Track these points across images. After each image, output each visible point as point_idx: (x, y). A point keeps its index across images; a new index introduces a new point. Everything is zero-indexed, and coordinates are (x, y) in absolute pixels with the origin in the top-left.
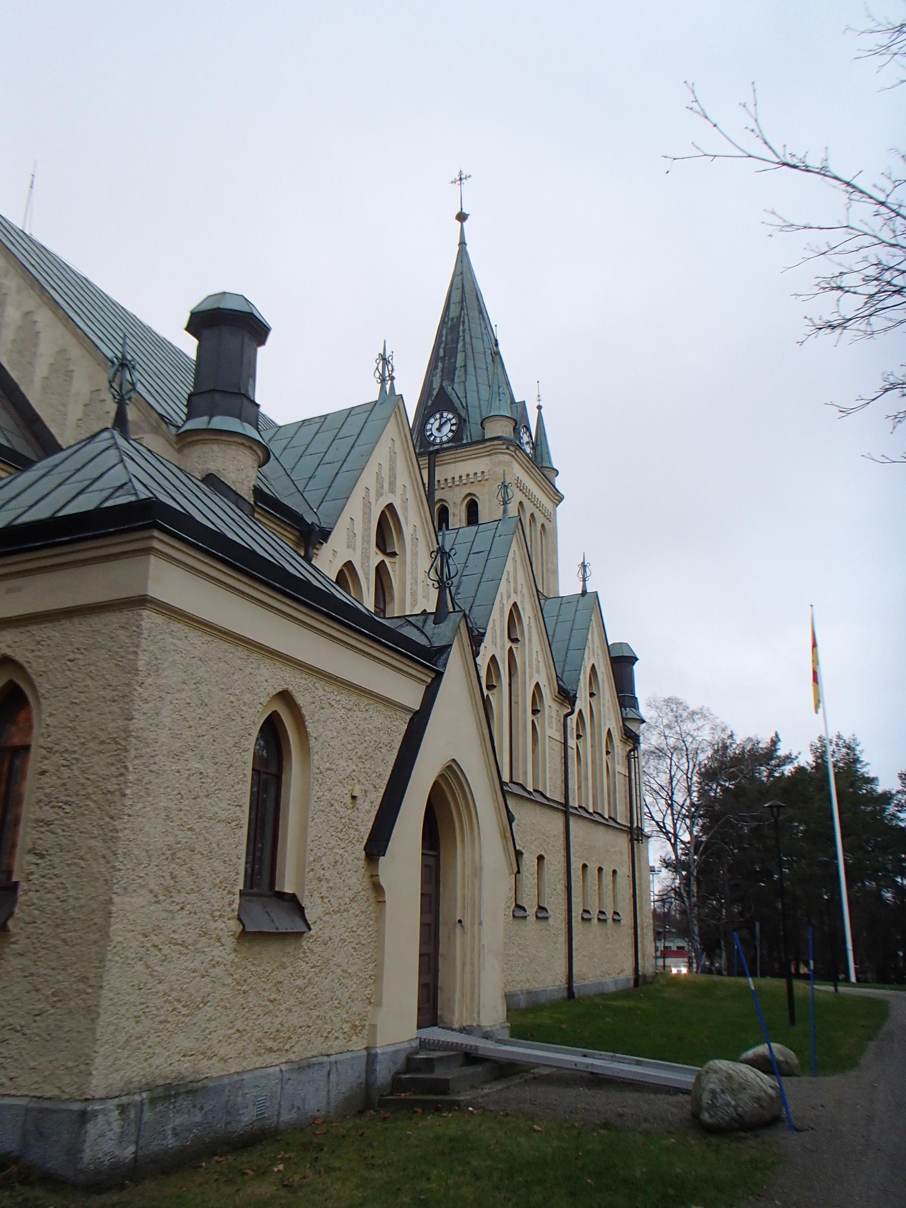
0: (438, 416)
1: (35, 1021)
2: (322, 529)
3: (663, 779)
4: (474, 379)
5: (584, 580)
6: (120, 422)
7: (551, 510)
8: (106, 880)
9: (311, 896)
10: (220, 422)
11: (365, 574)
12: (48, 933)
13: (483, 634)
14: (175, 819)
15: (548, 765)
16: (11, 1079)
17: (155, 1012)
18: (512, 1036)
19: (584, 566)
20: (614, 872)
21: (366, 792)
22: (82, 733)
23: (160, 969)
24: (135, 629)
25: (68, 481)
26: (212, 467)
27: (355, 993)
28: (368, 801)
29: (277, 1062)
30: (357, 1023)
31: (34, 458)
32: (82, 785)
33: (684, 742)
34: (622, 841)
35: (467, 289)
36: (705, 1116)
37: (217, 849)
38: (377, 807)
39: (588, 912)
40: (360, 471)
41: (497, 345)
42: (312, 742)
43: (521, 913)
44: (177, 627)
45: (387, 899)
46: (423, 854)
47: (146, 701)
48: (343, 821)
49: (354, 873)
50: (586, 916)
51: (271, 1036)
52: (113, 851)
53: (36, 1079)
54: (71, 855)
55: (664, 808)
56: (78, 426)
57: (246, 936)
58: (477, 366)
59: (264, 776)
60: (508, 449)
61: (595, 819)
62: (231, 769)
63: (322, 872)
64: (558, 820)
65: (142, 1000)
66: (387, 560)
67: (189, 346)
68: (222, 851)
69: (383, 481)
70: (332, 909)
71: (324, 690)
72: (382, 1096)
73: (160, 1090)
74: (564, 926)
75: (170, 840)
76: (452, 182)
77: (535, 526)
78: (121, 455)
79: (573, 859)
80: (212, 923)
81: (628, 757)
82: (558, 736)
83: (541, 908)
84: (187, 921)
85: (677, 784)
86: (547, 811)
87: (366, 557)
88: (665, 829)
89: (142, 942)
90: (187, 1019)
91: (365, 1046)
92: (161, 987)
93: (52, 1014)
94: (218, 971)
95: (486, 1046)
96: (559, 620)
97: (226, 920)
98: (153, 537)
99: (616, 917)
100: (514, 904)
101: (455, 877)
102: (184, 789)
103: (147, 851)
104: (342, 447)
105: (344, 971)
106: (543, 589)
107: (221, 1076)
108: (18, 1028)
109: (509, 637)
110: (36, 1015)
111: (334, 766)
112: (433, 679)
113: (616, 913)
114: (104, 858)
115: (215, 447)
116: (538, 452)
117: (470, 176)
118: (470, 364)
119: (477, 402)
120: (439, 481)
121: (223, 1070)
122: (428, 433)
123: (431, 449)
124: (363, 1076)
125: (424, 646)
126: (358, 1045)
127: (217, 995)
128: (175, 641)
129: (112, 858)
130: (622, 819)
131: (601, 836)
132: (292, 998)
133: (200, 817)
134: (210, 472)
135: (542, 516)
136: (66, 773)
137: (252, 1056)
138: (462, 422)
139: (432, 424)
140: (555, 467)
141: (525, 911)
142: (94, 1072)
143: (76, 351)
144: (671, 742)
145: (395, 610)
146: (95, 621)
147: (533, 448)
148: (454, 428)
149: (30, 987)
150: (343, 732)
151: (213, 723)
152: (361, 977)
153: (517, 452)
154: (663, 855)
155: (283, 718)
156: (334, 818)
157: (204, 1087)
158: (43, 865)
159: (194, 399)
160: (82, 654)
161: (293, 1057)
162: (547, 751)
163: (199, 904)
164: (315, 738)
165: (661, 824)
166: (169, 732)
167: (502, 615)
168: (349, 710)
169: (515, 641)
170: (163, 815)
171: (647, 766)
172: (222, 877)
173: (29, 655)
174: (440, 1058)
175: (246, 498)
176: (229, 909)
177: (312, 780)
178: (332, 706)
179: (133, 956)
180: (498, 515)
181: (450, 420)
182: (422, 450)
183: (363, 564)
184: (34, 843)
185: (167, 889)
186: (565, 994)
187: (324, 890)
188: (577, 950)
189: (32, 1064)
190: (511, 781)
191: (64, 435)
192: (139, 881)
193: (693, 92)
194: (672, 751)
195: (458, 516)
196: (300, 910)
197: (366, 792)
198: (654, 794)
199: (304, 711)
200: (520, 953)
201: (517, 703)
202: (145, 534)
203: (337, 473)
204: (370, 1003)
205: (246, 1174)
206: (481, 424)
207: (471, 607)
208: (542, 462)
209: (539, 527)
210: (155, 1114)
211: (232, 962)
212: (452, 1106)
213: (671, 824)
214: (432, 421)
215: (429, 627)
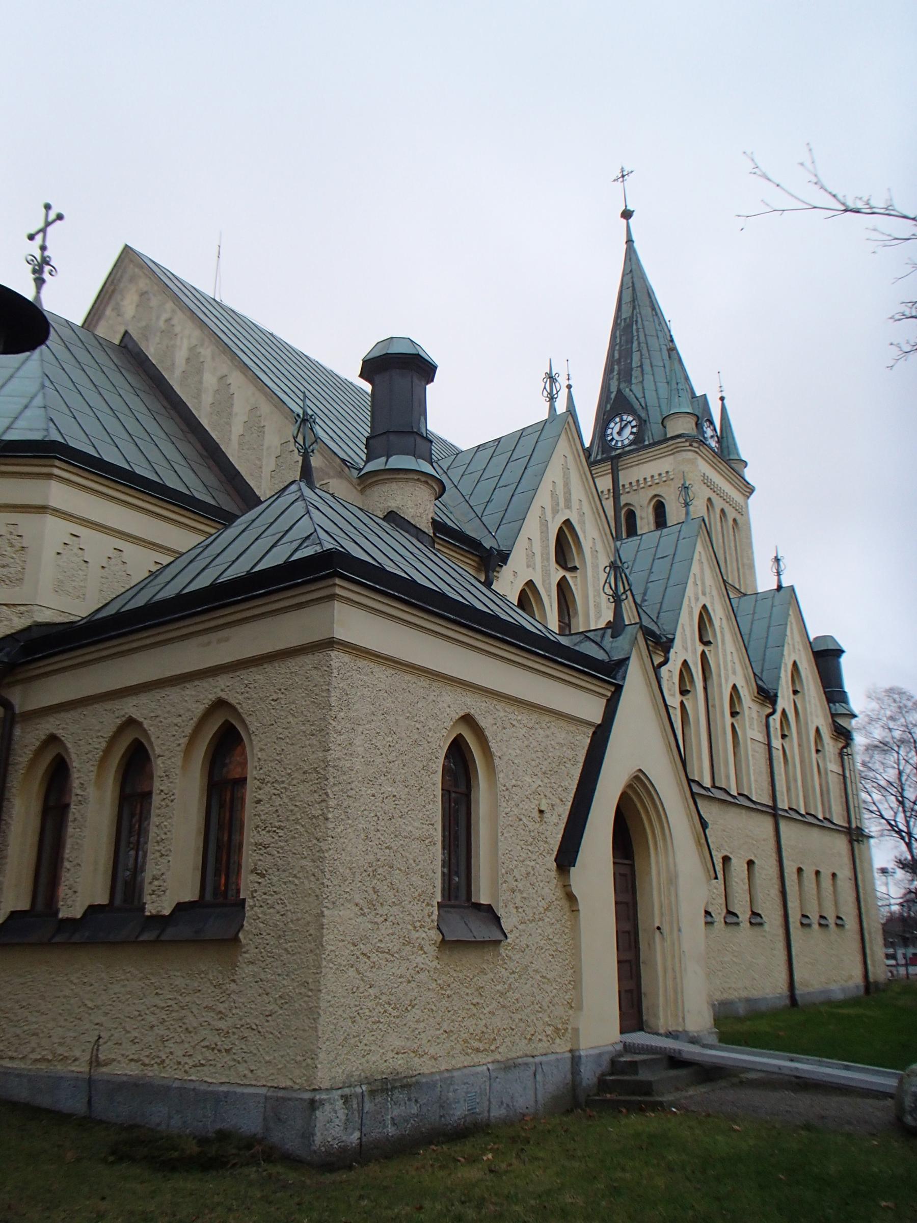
0: (617, 420)
1: (268, 1021)
2: (500, 552)
3: (891, 774)
4: (651, 378)
5: (779, 574)
6: (307, 473)
7: (742, 503)
8: (317, 896)
9: (506, 906)
10: (398, 461)
11: (546, 591)
12: (272, 943)
13: (672, 640)
14: (373, 839)
15: (752, 768)
16: (252, 1071)
17: (367, 1014)
18: (720, 1041)
19: (777, 560)
20: (834, 875)
21: (553, 805)
22: (288, 764)
23: (368, 974)
24: (326, 668)
25: (263, 536)
26: (393, 505)
27: (556, 998)
28: (555, 813)
29: (484, 1061)
30: (560, 1026)
31: (238, 513)
32: (292, 811)
33: (910, 733)
34: (841, 843)
35: (638, 286)
36: (909, 1120)
37: (414, 865)
38: (565, 820)
39: (807, 917)
40: (534, 491)
41: (672, 341)
42: (497, 761)
43: (734, 920)
44: (362, 663)
45: (581, 908)
46: (614, 863)
47: (340, 734)
48: (532, 834)
49: (546, 884)
50: (805, 921)
51: (477, 1037)
52: (321, 870)
53: (271, 1071)
54: (287, 874)
55: (895, 804)
56: (272, 477)
57: (446, 945)
58: (653, 364)
59: (453, 795)
60: (691, 445)
61: (807, 820)
62: (422, 790)
63: (515, 884)
64: (766, 824)
65: (357, 1003)
66: (568, 576)
67: (367, 387)
68: (419, 867)
69: (558, 498)
70: (526, 918)
71: (506, 711)
72: (589, 1096)
73: (378, 1083)
74: (781, 932)
75: (371, 857)
76: (614, 180)
77: (726, 520)
78: (307, 506)
79: (786, 862)
80: (413, 932)
81: (841, 755)
82: (761, 737)
83: (755, 914)
84: (391, 931)
85: (906, 780)
86: (753, 814)
87: (546, 574)
88: (897, 826)
89: (352, 951)
90: (398, 1021)
91: (568, 1049)
92: (371, 991)
93: (281, 1014)
94: (423, 976)
95: (689, 1050)
96: (755, 618)
97: (426, 930)
98: (335, 585)
99: (839, 922)
100: (725, 911)
101: (651, 884)
102: (379, 811)
103: (350, 869)
104: (516, 469)
105: (542, 977)
106: (740, 585)
107: (432, 1073)
108: (254, 1027)
109: (701, 640)
110: (267, 1016)
111: (519, 783)
112: (613, 693)
113: (839, 918)
114: (314, 876)
115: (394, 486)
116: (724, 445)
117: (632, 172)
118: (646, 362)
119: (656, 401)
120: (623, 486)
121: (433, 1067)
122: (609, 438)
123: (613, 454)
124: (569, 1076)
125: (602, 661)
126: (562, 1047)
127: (423, 998)
128: (361, 677)
129: (320, 875)
130: (839, 819)
131: (815, 837)
132: (494, 1002)
133: (396, 836)
134: (390, 510)
135: (733, 510)
136: (277, 801)
137: (460, 1055)
138: (642, 423)
139: (613, 428)
140: (744, 459)
141: (761, 917)
142: (319, 1066)
143: (265, 408)
144: (897, 734)
145: (579, 625)
146: (293, 664)
147: (718, 442)
148: (635, 430)
149: (261, 991)
150: (526, 751)
151: (402, 749)
152: (560, 983)
153: (701, 448)
154: (898, 855)
155: (468, 741)
156: (523, 832)
157: (417, 1083)
158: (265, 883)
159: (371, 441)
160: (283, 693)
161: (498, 1057)
162: (750, 753)
163: (401, 916)
164: (500, 758)
165: (893, 823)
166: (363, 760)
167: (691, 618)
168: (531, 728)
169: (707, 643)
170: (363, 836)
171: (872, 761)
172: (419, 890)
173: (240, 697)
174: (644, 1061)
175: (426, 530)
176: (429, 920)
177: (499, 797)
178: (514, 726)
179: (344, 963)
180: (682, 517)
181: (630, 422)
182: (604, 456)
183: (544, 581)
184: (256, 864)
185: (370, 902)
186: (787, 1002)
187: (518, 901)
188: (797, 955)
189: (267, 1058)
190: (714, 786)
191: (263, 488)
192: (345, 896)
193: (753, 160)
194: (899, 743)
195: (645, 520)
196: (497, 919)
197: (553, 805)
198: (882, 790)
199: (487, 733)
200: (734, 959)
201: (714, 706)
202: (330, 582)
203: (513, 495)
204: (571, 1007)
205: (459, 1161)
206: (662, 423)
207: (659, 613)
208: (729, 454)
209: (731, 522)
210: (375, 1105)
211: (435, 968)
212: (657, 1106)
213: (904, 822)
214: (612, 425)
215: (608, 641)
